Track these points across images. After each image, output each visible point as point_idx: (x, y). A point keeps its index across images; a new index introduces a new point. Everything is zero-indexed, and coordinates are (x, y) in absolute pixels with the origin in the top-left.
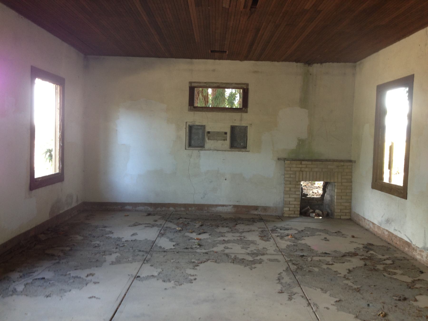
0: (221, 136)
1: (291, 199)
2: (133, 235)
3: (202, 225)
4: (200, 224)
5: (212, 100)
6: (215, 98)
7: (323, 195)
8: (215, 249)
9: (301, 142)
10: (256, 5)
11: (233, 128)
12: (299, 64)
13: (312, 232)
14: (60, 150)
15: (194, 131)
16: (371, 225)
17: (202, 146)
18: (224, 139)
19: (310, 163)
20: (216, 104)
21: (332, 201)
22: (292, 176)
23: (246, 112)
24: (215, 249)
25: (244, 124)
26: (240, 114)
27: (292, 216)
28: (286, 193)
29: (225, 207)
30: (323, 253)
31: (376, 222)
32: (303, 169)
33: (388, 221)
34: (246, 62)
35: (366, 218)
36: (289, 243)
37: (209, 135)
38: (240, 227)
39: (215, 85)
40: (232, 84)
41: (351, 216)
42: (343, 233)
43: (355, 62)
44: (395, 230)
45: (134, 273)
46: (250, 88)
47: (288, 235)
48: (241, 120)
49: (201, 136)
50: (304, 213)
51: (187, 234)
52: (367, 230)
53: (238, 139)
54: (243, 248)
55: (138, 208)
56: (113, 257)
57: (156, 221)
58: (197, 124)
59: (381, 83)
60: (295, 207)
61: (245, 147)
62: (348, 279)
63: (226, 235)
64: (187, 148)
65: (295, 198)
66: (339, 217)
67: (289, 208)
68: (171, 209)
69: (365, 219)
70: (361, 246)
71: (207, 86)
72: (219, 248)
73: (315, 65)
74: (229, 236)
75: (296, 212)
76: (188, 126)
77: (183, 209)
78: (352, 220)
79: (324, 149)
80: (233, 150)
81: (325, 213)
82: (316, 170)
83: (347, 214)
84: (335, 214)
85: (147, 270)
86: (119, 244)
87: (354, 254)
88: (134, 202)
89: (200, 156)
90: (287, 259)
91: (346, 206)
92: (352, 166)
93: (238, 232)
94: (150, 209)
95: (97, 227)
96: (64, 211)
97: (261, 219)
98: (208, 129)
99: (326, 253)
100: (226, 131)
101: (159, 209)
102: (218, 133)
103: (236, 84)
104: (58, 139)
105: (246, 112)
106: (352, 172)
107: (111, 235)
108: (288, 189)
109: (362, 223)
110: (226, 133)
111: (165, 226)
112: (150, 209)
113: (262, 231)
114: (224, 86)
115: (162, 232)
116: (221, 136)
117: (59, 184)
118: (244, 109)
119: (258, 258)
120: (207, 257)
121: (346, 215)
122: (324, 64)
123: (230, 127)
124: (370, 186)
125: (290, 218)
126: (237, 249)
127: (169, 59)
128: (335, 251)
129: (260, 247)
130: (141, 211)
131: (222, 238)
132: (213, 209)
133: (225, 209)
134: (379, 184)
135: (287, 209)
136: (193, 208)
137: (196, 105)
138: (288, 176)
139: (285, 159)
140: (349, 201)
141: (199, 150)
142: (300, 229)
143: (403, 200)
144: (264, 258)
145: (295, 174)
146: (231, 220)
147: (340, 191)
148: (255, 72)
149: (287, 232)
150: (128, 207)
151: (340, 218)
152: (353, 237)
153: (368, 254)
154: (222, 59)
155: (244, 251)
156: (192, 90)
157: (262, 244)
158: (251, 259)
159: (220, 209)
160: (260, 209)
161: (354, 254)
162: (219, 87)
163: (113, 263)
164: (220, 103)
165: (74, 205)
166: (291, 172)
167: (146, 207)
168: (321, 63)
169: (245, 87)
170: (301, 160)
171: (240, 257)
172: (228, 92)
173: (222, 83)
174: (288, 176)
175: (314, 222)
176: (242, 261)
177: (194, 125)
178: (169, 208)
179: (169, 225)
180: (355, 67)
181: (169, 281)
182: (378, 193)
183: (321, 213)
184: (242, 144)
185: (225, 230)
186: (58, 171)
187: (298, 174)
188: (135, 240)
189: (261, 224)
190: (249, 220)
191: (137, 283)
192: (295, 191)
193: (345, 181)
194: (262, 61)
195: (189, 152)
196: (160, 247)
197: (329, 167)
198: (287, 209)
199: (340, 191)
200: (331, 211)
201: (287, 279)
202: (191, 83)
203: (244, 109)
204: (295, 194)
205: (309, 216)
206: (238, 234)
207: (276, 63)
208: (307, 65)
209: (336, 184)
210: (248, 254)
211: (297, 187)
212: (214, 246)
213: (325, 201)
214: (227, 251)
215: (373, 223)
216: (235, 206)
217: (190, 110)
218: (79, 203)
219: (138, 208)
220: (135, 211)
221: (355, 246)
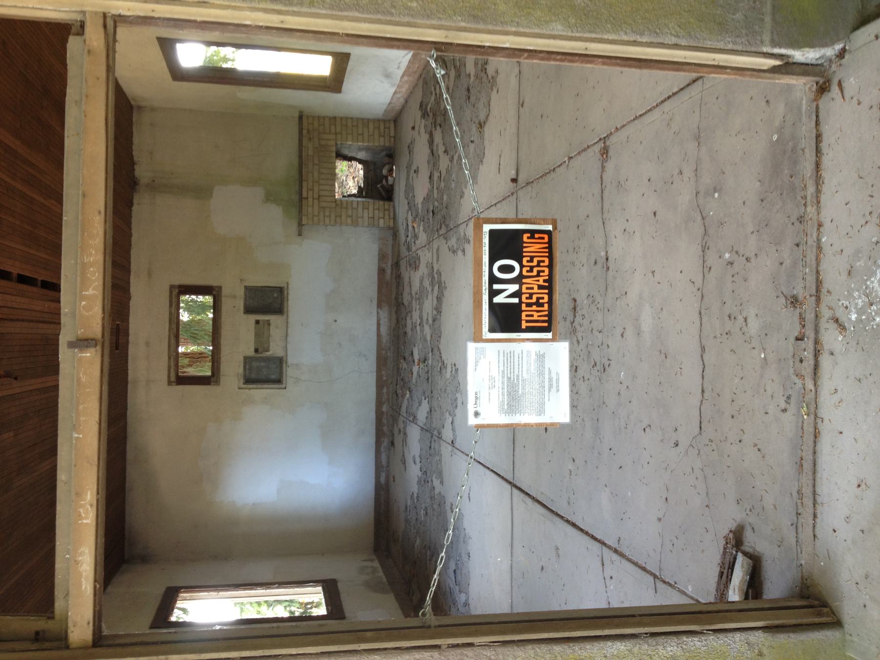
0: (261, 333)
1: (366, 215)
2: (415, 463)
3: (405, 359)
4: (402, 361)
5: (199, 345)
6: (194, 338)
7: (360, 161)
8: (429, 338)
9: (270, 197)
10: (36, 279)
11: (248, 310)
12: (135, 201)
13: (410, 188)
14: (285, 588)
15: (253, 376)
16: (398, 95)
17: (280, 362)
18: (266, 325)
19: (304, 184)
20: (206, 337)
21: (367, 149)
22: (327, 214)
23: (220, 288)
24: (429, 338)
25: (241, 292)
26: (223, 299)
27: (392, 214)
28: (355, 224)
29: (381, 322)
30: (430, 182)
31: (393, 90)
32: (316, 196)
33: (387, 76)
34: (132, 290)
35: (388, 101)
36: (421, 228)
37: (260, 350)
38: (406, 298)
39: (173, 341)
40: (170, 313)
41: (390, 121)
42: (409, 141)
43: (131, 107)
44: (399, 68)
45: (450, 448)
46: (177, 283)
47: (413, 227)
48: (234, 297)
49: (263, 364)
50: (387, 195)
51: (414, 381)
52: (406, 102)
53: (268, 302)
54: (427, 296)
55: (384, 462)
56: (436, 483)
57: (400, 431)
58: (241, 370)
59: (168, 76)
60: (378, 209)
61: (281, 290)
62: (452, 157)
63: (414, 321)
64: (283, 386)
65: (363, 209)
66: (392, 139)
67: (379, 218)
68: (384, 409)
69: (390, 103)
70: (423, 121)
71: (175, 356)
72: (427, 331)
73: (137, 173)
74: (416, 315)
75: (386, 207)
76: (245, 386)
77: (385, 390)
78: (393, 121)
79: (281, 159)
80: (285, 310)
81: (386, 160)
82: (316, 174)
83: (387, 126)
84: (387, 144)
85: (447, 434)
86: (424, 481)
87: (431, 135)
88: (374, 472)
89: (297, 365)
90: (436, 236)
91: (375, 128)
92: (308, 116)
93: (410, 303)
94: (385, 442)
95: (407, 521)
96: (384, 577)
97: (397, 265)
98: (251, 352)
99: (430, 177)
100: (254, 322)
101: (385, 429)
102: (258, 335)
103: (171, 305)
104: (268, 591)
105: (220, 288)
106: (319, 117)
107: (415, 495)
108: (349, 220)
109: (398, 106)
110: (257, 322)
111: (405, 415)
112: (385, 442)
113: (410, 265)
114: (174, 326)
115: (411, 419)
116: (261, 333)
117: (340, 585)
118: (214, 293)
119: (436, 276)
120: (436, 350)
121: (389, 128)
122: (135, 159)
123: (246, 316)
124: (338, 95)
125: (394, 218)
126: (428, 305)
127: (129, 420)
128: (428, 162)
129: (426, 271)
130: (388, 458)
131: (418, 327)
132: (384, 341)
133: (384, 321)
134: (334, 82)
135: (381, 221)
136: (383, 373)
137: (209, 373)
138: (327, 220)
139: (300, 224)
140: (365, 122)
141: (287, 366)
142: (407, 207)
143: (351, 57)
144: (436, 268)
145: (324, 208)
146: (397, 312)
147: (350, 137)
148: (150, 275)
149: (410, 228)
150: (383, 479)
151: (395, 137)
152: (413, 128)
153: (431, 115)
154: (128, 330)
155: (430, 297)
156: (183, 381)
157: (423, 269)
158: (437, 287)
159: (384, 330)
160: (384, 266)
161: (431, 135)
162: (176, 331)
163: (442, 483)
164: (205, 330)
165: (376, 564)
166: (322, 214)
167: (382, 449)
168: (133, 163)
169: (177, 291)
170: (301, 198)
171: (435, 302)
172: (185, 317)
173: (169, 331)
174: (327, 220)
175: (399, 179)
176: (439, 299)
177: (245, 376)
178: (383, 413)
179: (404, 409)
180: (140, 108)
181: (456, 400)
182: (345, 86)
183: (387, 167)
184: (276, 295)
185: (409, 322)
186: (320, 588)
187: (324, 204)
188: (420, 457)
189: (403, 264)
190: (398, 284)
191: (456, 445)
192: (352, 209)
193: (333, 128)
194: (129, 262)
195: (289, 381)
196: (427, 418)
197: (311, 153)
198: (381, 221)
199: (350, 137)
200: (383, 151)
201: (453, 242)
202: (170, 383)
203: (214, 293)
204: (357, 208)
205: (392, 186)
206: (414, 302)
207: (134, 239)
208: (137, 187)
209: (339, 142)
210: (432, 290)
211: (345, 205)
212: (425, 340)
213: (368, 159)
214: (430, 321)
215: (395, 93)
216: (379, 306)
217: (217, 382)
218: (375, 557)
219: (384, 462)
220: (388, 466)
221: (422, 130)
